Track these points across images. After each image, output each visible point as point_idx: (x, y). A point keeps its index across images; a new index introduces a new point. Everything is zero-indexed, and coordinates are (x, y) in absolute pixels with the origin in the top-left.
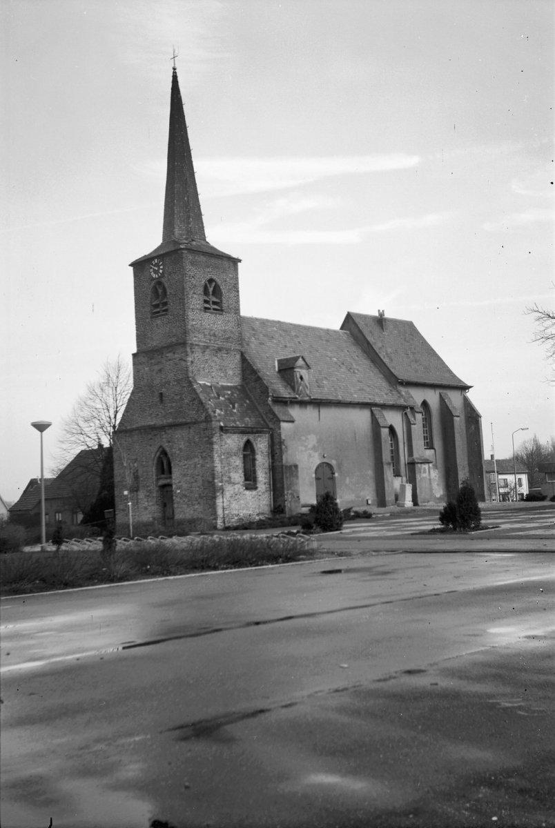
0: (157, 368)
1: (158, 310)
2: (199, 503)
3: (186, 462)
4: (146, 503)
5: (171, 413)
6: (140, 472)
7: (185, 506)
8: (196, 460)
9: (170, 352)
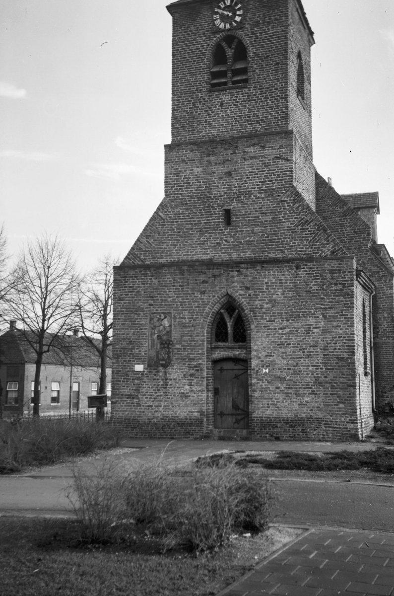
0: (221, 169)
1: (223, 80)
2: (313, 393)
3: (285, 323)
4: (187, 387)
5: (249, 243)
6: (175, 335)
7: (281, 397)
8: (311, 321)
9: (254, 145)
